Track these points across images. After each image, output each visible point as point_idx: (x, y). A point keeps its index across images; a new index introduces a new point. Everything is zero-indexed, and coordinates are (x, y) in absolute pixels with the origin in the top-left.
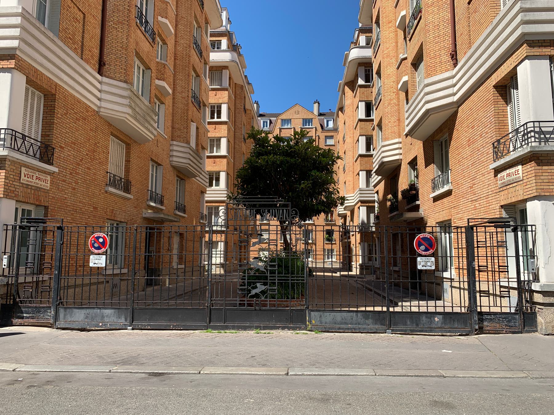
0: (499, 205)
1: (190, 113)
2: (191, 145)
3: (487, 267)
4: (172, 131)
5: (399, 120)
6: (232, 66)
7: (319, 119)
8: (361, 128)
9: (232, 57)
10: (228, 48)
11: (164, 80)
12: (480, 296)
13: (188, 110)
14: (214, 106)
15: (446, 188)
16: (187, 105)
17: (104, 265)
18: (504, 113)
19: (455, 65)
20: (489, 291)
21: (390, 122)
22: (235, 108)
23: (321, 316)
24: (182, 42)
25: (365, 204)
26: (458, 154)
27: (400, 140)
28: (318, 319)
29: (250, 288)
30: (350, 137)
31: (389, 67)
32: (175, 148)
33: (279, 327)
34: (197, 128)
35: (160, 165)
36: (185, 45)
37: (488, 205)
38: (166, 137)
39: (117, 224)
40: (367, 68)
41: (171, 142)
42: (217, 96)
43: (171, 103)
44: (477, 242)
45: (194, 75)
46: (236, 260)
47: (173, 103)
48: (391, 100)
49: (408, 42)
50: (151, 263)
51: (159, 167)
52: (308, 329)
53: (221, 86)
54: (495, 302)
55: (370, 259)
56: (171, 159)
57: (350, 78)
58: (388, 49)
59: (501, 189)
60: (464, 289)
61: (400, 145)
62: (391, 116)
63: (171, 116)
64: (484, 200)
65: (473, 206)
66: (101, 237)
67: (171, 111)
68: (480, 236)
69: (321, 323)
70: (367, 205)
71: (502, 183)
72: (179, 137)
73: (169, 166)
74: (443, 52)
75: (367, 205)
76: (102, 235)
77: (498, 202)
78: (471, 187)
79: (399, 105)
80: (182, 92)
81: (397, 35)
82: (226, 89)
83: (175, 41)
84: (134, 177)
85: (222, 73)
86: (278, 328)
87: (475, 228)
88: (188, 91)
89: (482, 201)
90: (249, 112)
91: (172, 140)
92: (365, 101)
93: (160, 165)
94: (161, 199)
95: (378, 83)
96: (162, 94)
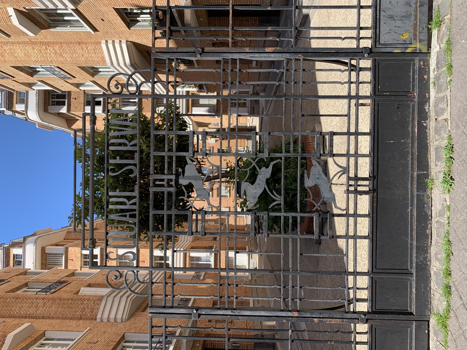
2: (104, 294)
4: (84, 319)
5: (79, 43)
6: (41, 243)
9: (31, 243)
10: (21, 247)
11: (5, 336)
13: (60, 299)
14: (85, 262)
16: (54, 300)
21: (83, 55)
23: (391, 17)
25: (190, 108)
27: (103, 42)
28: (398, 23)
29: (317, 206)
31: (16, 55)
32: (106, 316)
33: (420, 124)
34: (89, 286)
35: (123, 337)
38: (88, 328)
40: (51, 103)
41: (99, 320)
42: (74, 258)
43: (48, 320)
45: (25, 289)
46: (244, 238)
47: (49, 318)
48: (56, 53)
50: (247, 347)
51: (127, 338)
52: (424, 50)
53: (62, 254)
55: (244, 105)
56: (119, 321)
57: (63, 122)
61: (110, 42)
62: (76, 53)
63: (64, 321)
69: (408, 16)
70: (190, 106)
73: (128, 323)
75: (190, 106)
79: (61, 43)
80: (37, 306)
82: (67, 249)
85: (49, 254)
86: (423, 130)
88: (37, 299)
90: (98, 225)
92: (84, 106)
93: (123, 337)
95: (43, 74)
96: (29, 337)
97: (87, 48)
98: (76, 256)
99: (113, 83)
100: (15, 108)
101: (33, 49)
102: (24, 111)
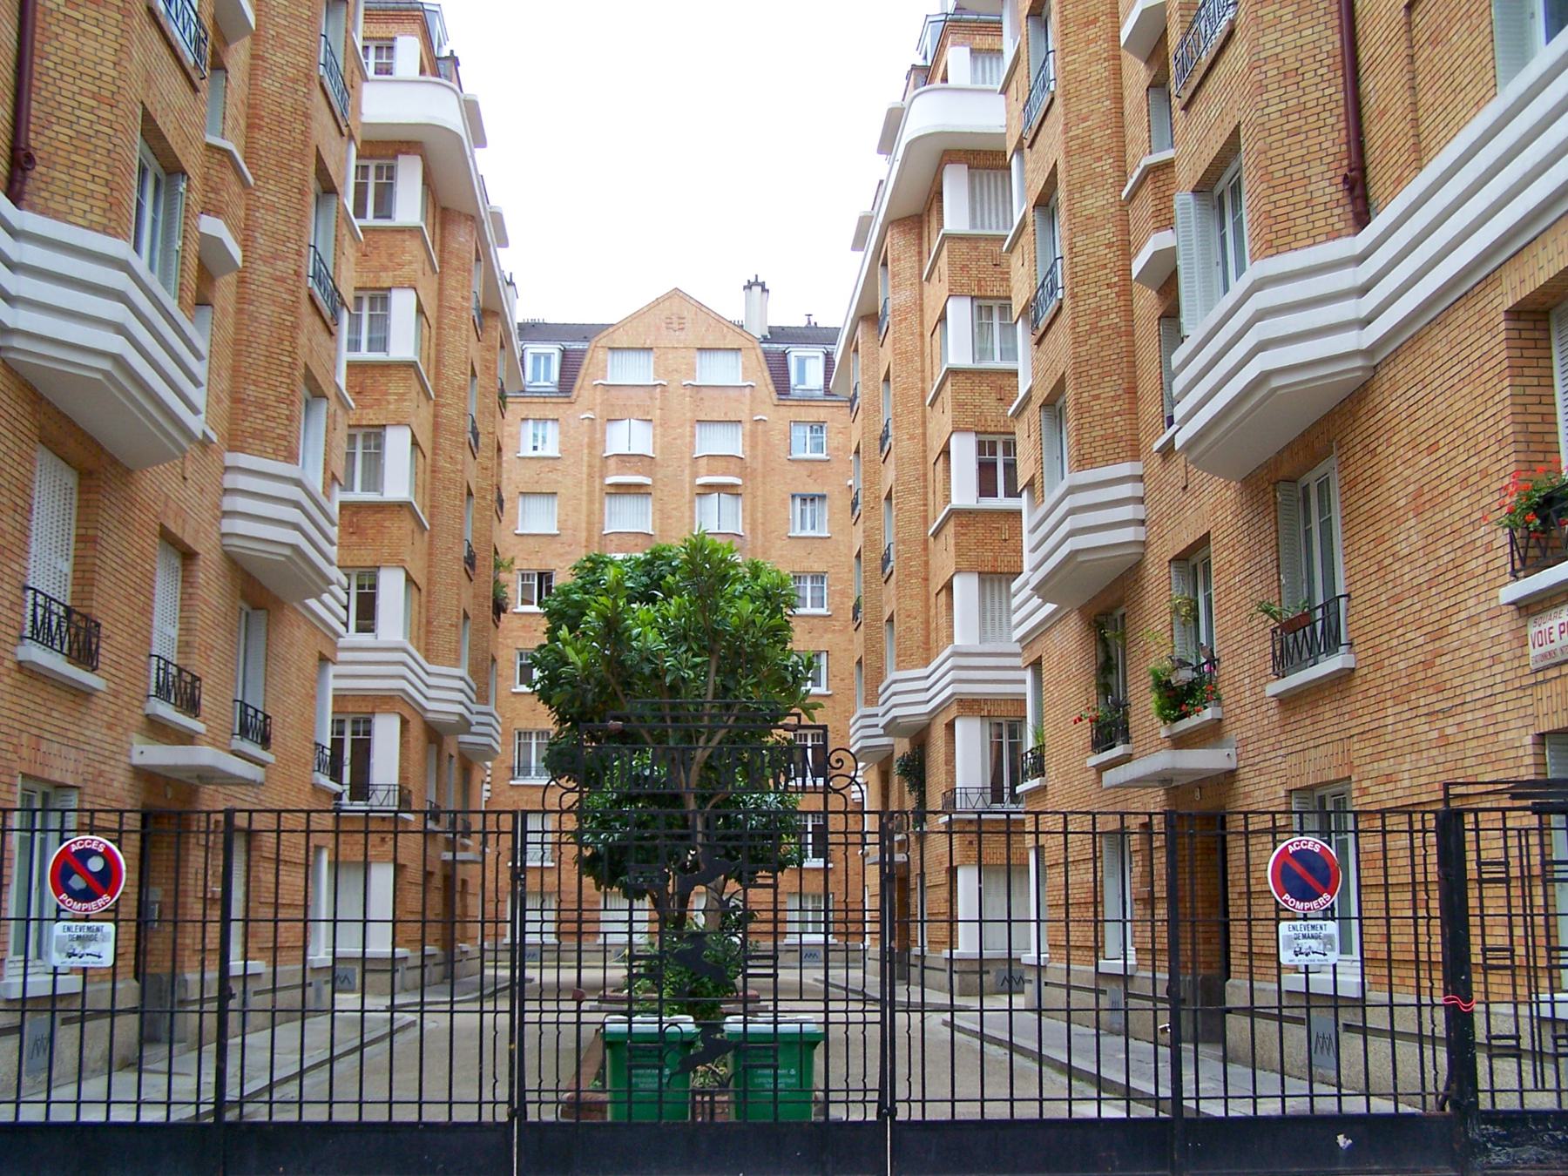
0: (1532, 731)
1: (302, 339)
3: (1512, 951)
7: (766, 353)
8: (959, 406)
12: (1517, 1038)
13: (295, 327)
15: (1329, 665)
17: (108, 960)
18: (1544, 409)
19: (1362, 218)
20: (1490, 1058)
21: (1096, 397)
22: (440, 306)
24: (279, 57)
26: (1379, 541)
30: (912, 437)
31: (1089, 190)
36: (292, 72)
37: (1491, 730)
39: (46, 796)
44: (1479, 863)
48: (1099, 313)
49: (1178, 114)
54: (1539, 1078)
58: (1085, 120)
59: (1540, 677)
60: (1434, 1039)
64: (1478, 714)
65: (1435, 734)
66: (94, 853)
67: (231, 330)
68: (1487, 844)
71: (1544, 656)
72: (259, 435)
74: (1318, 168)
76: (99, 842)
77: (1529, 721)
78: (1427, 664)
80: (276, 256)
81: (1117, 72)
83: (253, 57)
84: (109, 610)
87: (1470, 818)
89: (1469, 717)
91: (232, 449)
94: (193, 694)
97: (1118, 414)
98: (385, 269)
99: (842, 754)
100: (954, 45)
101: (1109, 245)
102: (945, 80)
